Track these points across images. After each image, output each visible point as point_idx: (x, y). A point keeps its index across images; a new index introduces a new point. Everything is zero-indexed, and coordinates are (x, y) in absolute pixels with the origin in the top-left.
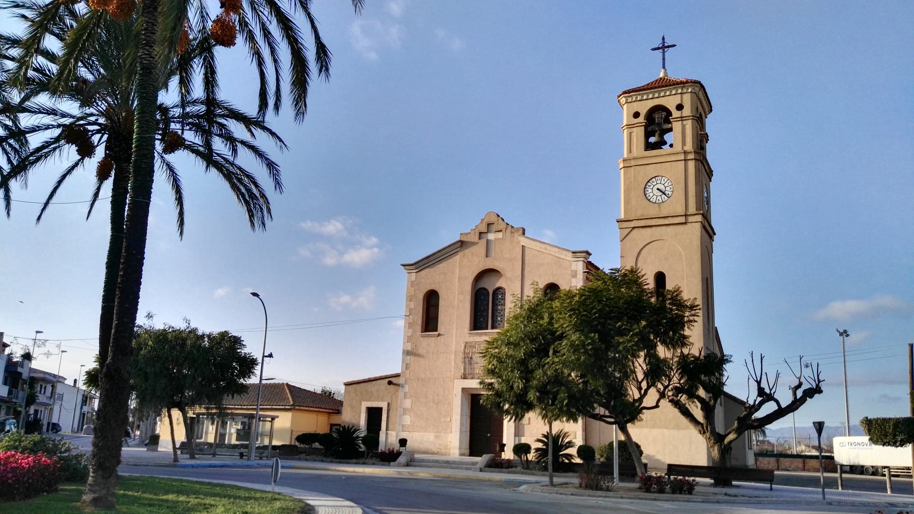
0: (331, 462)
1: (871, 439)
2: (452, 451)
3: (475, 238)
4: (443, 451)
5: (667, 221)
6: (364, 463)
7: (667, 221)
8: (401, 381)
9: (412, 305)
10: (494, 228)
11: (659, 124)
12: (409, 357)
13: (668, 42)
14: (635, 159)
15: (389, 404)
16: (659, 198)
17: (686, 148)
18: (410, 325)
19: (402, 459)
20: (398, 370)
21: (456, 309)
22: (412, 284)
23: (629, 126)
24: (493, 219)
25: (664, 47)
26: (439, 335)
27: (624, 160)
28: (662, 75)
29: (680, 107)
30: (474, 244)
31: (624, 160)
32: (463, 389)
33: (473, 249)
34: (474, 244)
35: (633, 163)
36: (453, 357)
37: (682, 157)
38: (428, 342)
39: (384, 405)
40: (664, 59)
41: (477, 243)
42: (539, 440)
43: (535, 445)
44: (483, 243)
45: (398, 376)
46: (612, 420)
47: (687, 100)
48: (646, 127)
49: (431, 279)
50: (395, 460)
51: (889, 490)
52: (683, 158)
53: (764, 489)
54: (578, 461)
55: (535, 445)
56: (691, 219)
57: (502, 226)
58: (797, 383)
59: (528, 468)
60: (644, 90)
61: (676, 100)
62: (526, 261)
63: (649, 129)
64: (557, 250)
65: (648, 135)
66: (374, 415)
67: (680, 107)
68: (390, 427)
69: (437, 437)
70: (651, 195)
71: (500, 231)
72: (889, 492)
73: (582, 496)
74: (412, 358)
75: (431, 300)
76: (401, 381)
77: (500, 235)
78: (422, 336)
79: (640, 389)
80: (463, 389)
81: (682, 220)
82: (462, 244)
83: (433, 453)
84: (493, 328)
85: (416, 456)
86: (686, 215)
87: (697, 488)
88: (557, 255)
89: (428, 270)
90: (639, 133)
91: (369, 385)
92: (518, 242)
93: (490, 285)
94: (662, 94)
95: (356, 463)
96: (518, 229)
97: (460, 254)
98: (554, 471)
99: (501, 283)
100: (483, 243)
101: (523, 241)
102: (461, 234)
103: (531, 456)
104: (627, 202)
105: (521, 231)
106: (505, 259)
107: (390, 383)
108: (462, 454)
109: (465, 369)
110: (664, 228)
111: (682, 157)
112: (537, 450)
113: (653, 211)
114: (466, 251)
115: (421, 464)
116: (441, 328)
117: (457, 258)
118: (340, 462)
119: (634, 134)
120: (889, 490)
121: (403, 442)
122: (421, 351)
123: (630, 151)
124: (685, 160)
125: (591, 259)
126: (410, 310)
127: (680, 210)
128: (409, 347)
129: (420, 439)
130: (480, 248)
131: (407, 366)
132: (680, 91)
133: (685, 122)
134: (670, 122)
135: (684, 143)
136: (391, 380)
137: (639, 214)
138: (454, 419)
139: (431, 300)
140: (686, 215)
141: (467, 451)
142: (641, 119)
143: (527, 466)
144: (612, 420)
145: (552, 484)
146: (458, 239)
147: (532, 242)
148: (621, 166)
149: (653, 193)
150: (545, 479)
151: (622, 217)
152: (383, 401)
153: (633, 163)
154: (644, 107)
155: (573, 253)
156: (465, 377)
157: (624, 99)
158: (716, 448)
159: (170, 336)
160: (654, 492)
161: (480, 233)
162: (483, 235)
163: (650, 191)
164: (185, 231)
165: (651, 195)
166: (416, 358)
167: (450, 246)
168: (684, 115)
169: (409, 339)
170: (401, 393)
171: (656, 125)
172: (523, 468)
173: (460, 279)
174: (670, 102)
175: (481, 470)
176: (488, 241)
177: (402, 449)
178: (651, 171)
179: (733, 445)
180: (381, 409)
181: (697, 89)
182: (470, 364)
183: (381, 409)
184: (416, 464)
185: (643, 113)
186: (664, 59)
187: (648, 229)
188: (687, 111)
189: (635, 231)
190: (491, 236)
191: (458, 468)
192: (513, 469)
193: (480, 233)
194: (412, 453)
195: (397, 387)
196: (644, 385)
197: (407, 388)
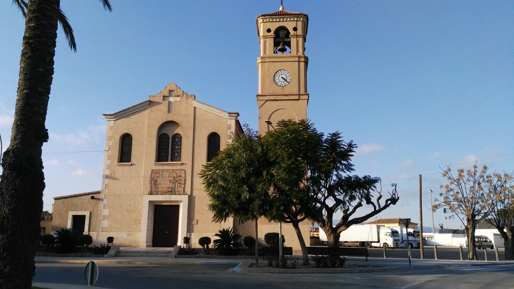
0: (54, 256)
2: (140, 245)
3: (160, 100)
4: (134, 244)
5: (287, 98)
6: (81, 256)
7: (287, 98)
8: (101, 196)
9: (111, 143)
10: (174, 94)
11: (282, 38)
12: (108, 180)
14: (268, 57)
15: (91, 213)
16: (283, 83)
17: (299, 54)
18: (109, 157)
19: (112, 252)
20: (99, 189)
21: (145, 148)
22: (111, 128)
23: (265, 37)
24: (173, 87)
26: (132, 165)
27: (262, 58)
28: (281, 9)
29: (295, 29)
30: (158, 103)
31: (262, 58)
32: (150, 202)
33: (159, 107)
34: (158, 103)
35: (267, 60)
36: (142, 180)
37: (297, 59)
38: (123, 170)
39: (87, 214)
41: (162, 103)
42: (217, 235)
43: (213, 238)
44: (166, 103)
45: (99, 193)
46: (288, 220)
47: (300, 26)
48: (275, 39)
49: (125, 126)
50: (106, 253)
51: (461, 258)
52: (297, 60)
53: (363, 260)
54: (244, 247)
55: (213, 238)
56: (302, 97)
57: (180, 93)
58: (379, 196)
59: (208, 254)
60: (275, 15)
61: (293, 24)
62: (197, 117)
63: (276, 40)
64: (218, 111)
65: (276, 44)
66: (79, 220)
67: (295, 29)
68: (92, 229)
69: (129, 235)
70: (278, 81)
71: (179, 96)
72: (422, 259)
73: (287, 273)
74: (111, 180)
75: (126, 142)
76: (101, 196)
77: (178, 99)
79: (324, 195)
80: (150, 202)
81: (296, 97)
82: (150, 103)
83: (126, 246)
84: (171, 161)
85: (121, 249)
86: (299, 95)
87: (346, 263)
88: (218, 114)
89: (123, 119)
90: (270, 42)
91: (74, 200)
92: (191, 105)
93: (170, 132)
94: (285, 20)
95: (75, 256)
96: (191, 96)
97: (149, 110)
98: (259, 255)
99: (178, 131)
100: (166, 103)
101: (195, 104)
102: (150, 96)
103: (211, 246)
104: (263, 84)
105: (193, 97)
106: (182, 113)
107: (93, 198)
108: (147, 246)
109: (151, 188)
110: (285, 101)
111: (297, 59)
113: (279, 91)
114: (153, 108)
115: (118, 254)
116: (134, 158)
117: (146, 112)
118: (61, 256)
119: (267, 43)
120: (461, 258)
121: (110, 239)
122: (117, 176)
123: (265, 52)
124: (299, 61)
125: (239, 118)
126: (110, 148)
127: (296, 91)
128: (108, 173)
129: (121, 238)
130: (164, 106)
131: (106, 186)
132: (295, 19)
133: (298, 39)
134: (289, 38)
135: (298, 52)
136: (94, 196)
137: (270, 92)
138: (142, 222)
139: (126, 142)
140: (299, 95)
141: (151, 244)
142: (272, 33)
143: (208, 253)
144: (288, 220)
146: (147, 99)
147: (201, 105)
148: (260, 61)
149: (279, 80)
151: (260, 93)
152: (86, 210)
153: (267, 60)
154: (274, 26)
155: (229, 113)
156: (151, 193)
157: (261, 20)
158: (332, 236)
159: (28, 62)
160: (329, 267)
161: (164, 96)
162: (166, 98)
163: (277, 78)
165: (278, 81)
166: (114, 181)
167: (141, 104)
168: (298, 34)
169: (108, 167)
170: (101, 205)
171: (281, 39)
172: (205, 254)
173: (148, 126)
174: (290, 25)
176: (169, 102)
177: (110, 244)
178: (278, 66)
179: (283, 234)
180: (85, 216)
181: (305, 20)
182: (155, 184)
183: (85, 216)
184: (123, 254)
185: (273, 30)
187: (276, 102)
188: (300, 32)
189: (268, 102)
190: (171, 99)
191: (155, 256)
192: (197, 255)
193: (164, 96)
194: (119, 246)
195: (98, 201)
196: (326, 195)
197: (105, 202)
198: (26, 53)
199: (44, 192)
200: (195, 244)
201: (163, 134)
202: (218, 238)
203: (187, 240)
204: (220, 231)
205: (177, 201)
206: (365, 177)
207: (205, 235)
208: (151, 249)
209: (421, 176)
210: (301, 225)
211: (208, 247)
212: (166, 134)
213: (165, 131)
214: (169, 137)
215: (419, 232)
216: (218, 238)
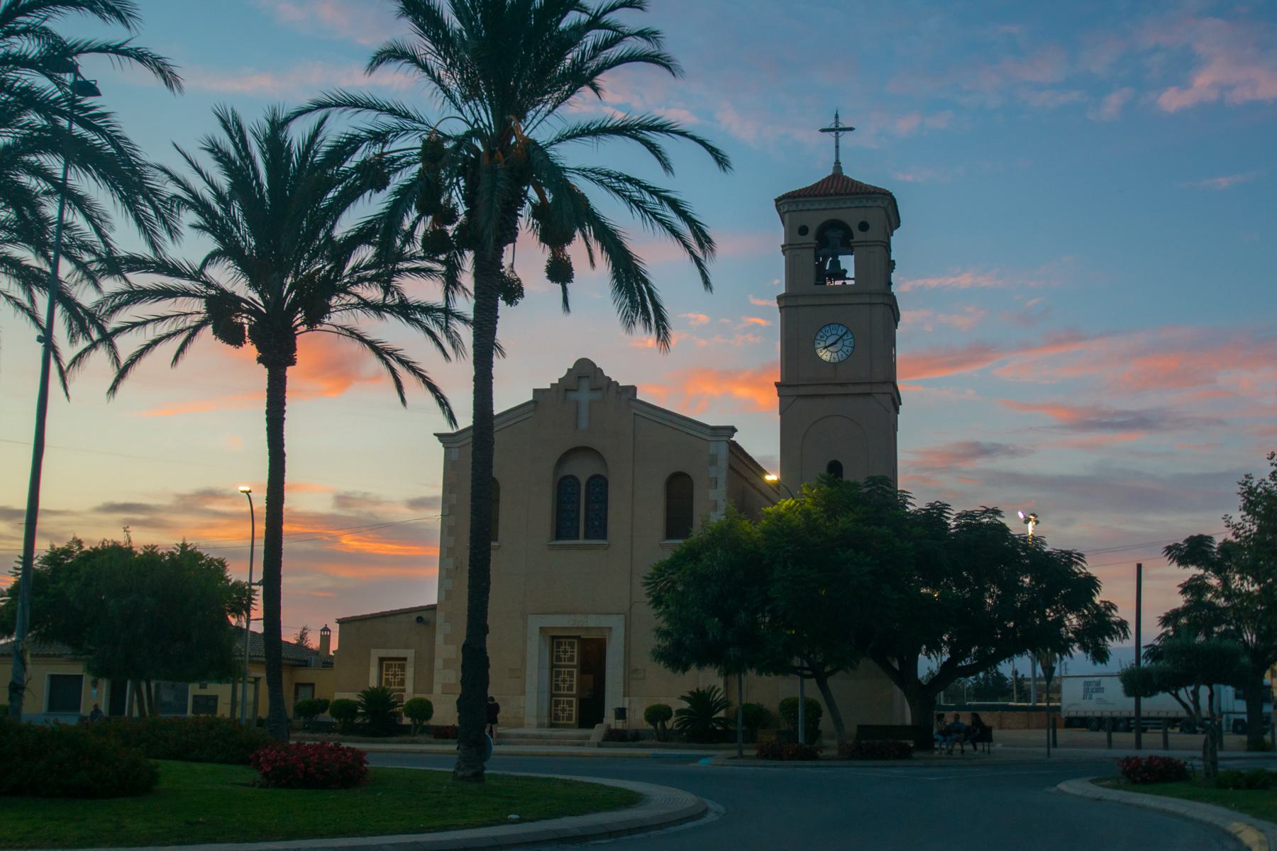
1: (362, 762)
13: (844, 123)
25: (837, 130)
29: (864, 227)
40: (837, 147)
46: (809, 673)
67: (864, 227)
78: (552, 547)
84: (586, 537)
93: (583, 470)
103: (670, 724)
112: (680, 712)
141: (546, 721)
142: (810, 238)
143: (665, 737)
144: (809, 673)
145: (742, 756)
150: (735, 753)
153: (801, 301)
154: (814, 221)
164: (406, 397)
175: (599, 746)
180: (53, 678)
183: (53, 678)
186: (837, 147)
198: (81, 547)
199: (563, 374)
200: (637, 718)
201: (565, 478)
202: (686, 705)
203: (621, 713)
204: (691, 693)
205: (601, 629)
206: (685, 668)
207: (664, 701)
208: (545, 732)
209: (1139, 566)
210: (831, 682)
211: (663, 725)
212: (573, 477)
213: (568, 470)
214: (579, 484)
215: (1086, 683)
216: (686, 705)
